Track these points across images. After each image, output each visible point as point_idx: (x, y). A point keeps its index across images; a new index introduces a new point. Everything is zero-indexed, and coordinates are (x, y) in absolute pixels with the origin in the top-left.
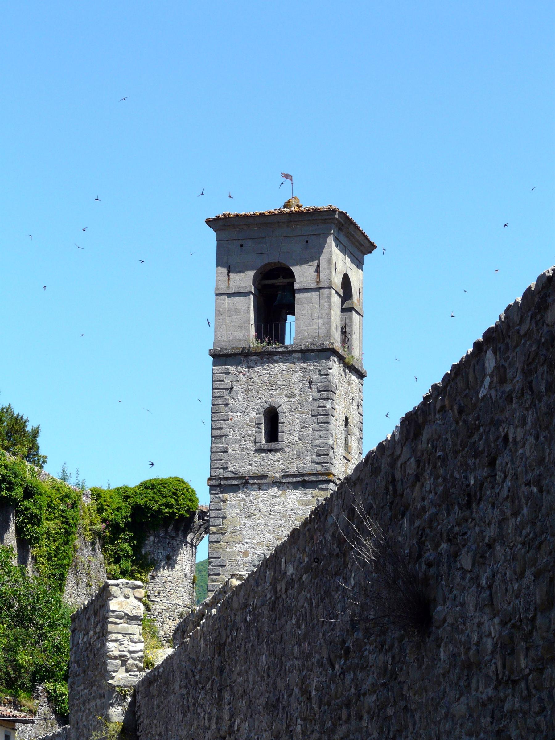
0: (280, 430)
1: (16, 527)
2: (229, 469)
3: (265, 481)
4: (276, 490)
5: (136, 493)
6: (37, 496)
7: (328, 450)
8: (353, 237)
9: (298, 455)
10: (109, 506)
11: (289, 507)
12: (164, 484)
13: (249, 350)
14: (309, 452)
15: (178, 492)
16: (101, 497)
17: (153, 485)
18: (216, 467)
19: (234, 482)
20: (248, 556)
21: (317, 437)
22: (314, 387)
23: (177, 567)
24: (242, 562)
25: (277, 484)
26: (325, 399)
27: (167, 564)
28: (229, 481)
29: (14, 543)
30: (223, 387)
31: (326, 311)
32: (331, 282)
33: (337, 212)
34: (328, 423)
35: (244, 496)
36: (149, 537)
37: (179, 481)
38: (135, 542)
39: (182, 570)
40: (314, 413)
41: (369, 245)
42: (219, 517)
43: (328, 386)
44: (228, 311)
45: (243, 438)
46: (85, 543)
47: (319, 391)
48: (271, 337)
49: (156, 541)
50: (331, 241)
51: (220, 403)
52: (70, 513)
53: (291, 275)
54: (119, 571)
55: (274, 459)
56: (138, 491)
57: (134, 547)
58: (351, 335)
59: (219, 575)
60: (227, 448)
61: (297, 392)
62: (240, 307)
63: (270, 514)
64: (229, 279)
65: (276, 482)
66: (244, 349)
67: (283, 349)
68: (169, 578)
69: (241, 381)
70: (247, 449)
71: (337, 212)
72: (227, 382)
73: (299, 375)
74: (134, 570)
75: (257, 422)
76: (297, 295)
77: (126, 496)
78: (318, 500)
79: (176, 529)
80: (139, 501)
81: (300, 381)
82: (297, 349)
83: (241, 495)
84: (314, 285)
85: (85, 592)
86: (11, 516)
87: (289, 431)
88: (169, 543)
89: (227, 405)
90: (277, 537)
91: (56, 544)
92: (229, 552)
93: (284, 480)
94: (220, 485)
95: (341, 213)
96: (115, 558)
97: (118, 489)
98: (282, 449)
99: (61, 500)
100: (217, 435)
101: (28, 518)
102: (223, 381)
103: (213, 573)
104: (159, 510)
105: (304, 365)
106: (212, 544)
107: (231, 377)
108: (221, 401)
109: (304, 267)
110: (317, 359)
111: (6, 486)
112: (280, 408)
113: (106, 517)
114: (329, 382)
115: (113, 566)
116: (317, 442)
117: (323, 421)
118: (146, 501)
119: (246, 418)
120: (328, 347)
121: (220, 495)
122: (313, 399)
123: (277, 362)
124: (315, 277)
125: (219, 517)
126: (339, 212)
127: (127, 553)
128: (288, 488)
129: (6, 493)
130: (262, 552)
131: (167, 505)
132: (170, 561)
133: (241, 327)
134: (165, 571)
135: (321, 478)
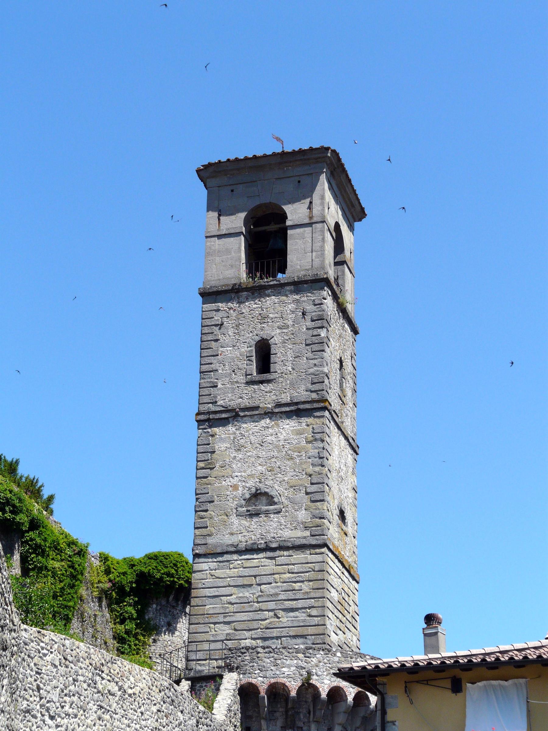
0: (272, 362)
1: (21, 556)
2: (219, 403)
3: (257, 412)
4: (268, 421)
5: (141, 562)
6: (41, 529)
7: (323, 377)
8: (345, 191)
9: (292, 384)
10: (116, 570)
11: (282, 437)
12: (166, 556)
13: (240, 285)
14: (303, 381)
15: (178, 564)
16: (108, 560)
17: (156, 556)
18: (205, 402)
19: (224, 416)
20: (238, 490)
21: (312, 366)
22: (308, 318)
23: (177, 633)
24: (231, 496)
25: (269, 414)
26: (319, 328)
27: (167, 629)
28: (218, 415)
29: (18, 571)
30: (213, 323)
31: (319, 244)
32: (324, 216)
33: (330, 151)
34: (323, 351)
35: (234, 429)
36: (153, 604)
37: (179, 554)
38: (139, 607)
39: (181, 637)
40: (308, 342)
41: (359, 208)
42: (208, 452)
43: (323, 315)
44: (219, 251)
45: (234, 371)
46: (92, 598)
47: (313, 321)
48: (262, 271)
49: (158, 608)
50: (323, 178)
51: (209, 339)
52: (76, 559)
53: (284, 216)
54: (124, 630)
55: (266, 390)
56: (143, 561)
57: (137, 611)
58: (344, 287)
59: (206, 511)
60: (216, 383)
61: (290, 323)
62: (231, 247)
63: (262, 446)
64: (219, 223)
65: (269, 412)
66: (235, 284)
67: (275, 282)
68: (169, 642)
69: (232, 316)
70: (237, 382)
71: (330, 151)
72: (217, 318)
73: (292, 306)
74: (138, 633)
75: (248, 355)
76: (290, 232)
77: (132, 565)
78: (313, 428)
79: (176, 599)
80: (143, 569)
81: (293, 312)
82: (289, 281)
83: (231, 428)
84: (307, 221)
85: (91, 642)
86: (16, 545)
87: (282, 361)
88: (170, 611)
89: (217, 340)
90: (269, 469)
91: (62, 584)
92: (218, 487)
93: (277, 410)
94: (208, 420)
95: (334, 151)
96: (120, 619)
97: (125, 559)
98: (275, 379)
99: (69, 545)
100: (207, 370)
101: (32, 548)
102: (213, 318)
103: (201, 509)
104: (161, 578)
105: (297, 297)
106: (199, 480)
107: (220, 314)
108: (210, 337)
109: (297, 205)
110: (310, 290)
111: (9, 509)
112: (272, 340)
113: (112, 578)
114: (323, 310)
115: (118, 626)
116: (311, 370)
117: (317, 349)
118: (150, 570)
119: (235, 352)
120: (322, 277)
121: (209, 430)
122: (307, 329)
123: (269, 296)
124: (307, 214)
125: (208, 452)
126: (332, 150)
127: (132, 615)
128: (281, 418)
129: (9, 516)
130: (254, 485)
131: (169, 574)
132: (171, 628)
133: (232, 266)
134: (166, 636)
135: (316, 405)
